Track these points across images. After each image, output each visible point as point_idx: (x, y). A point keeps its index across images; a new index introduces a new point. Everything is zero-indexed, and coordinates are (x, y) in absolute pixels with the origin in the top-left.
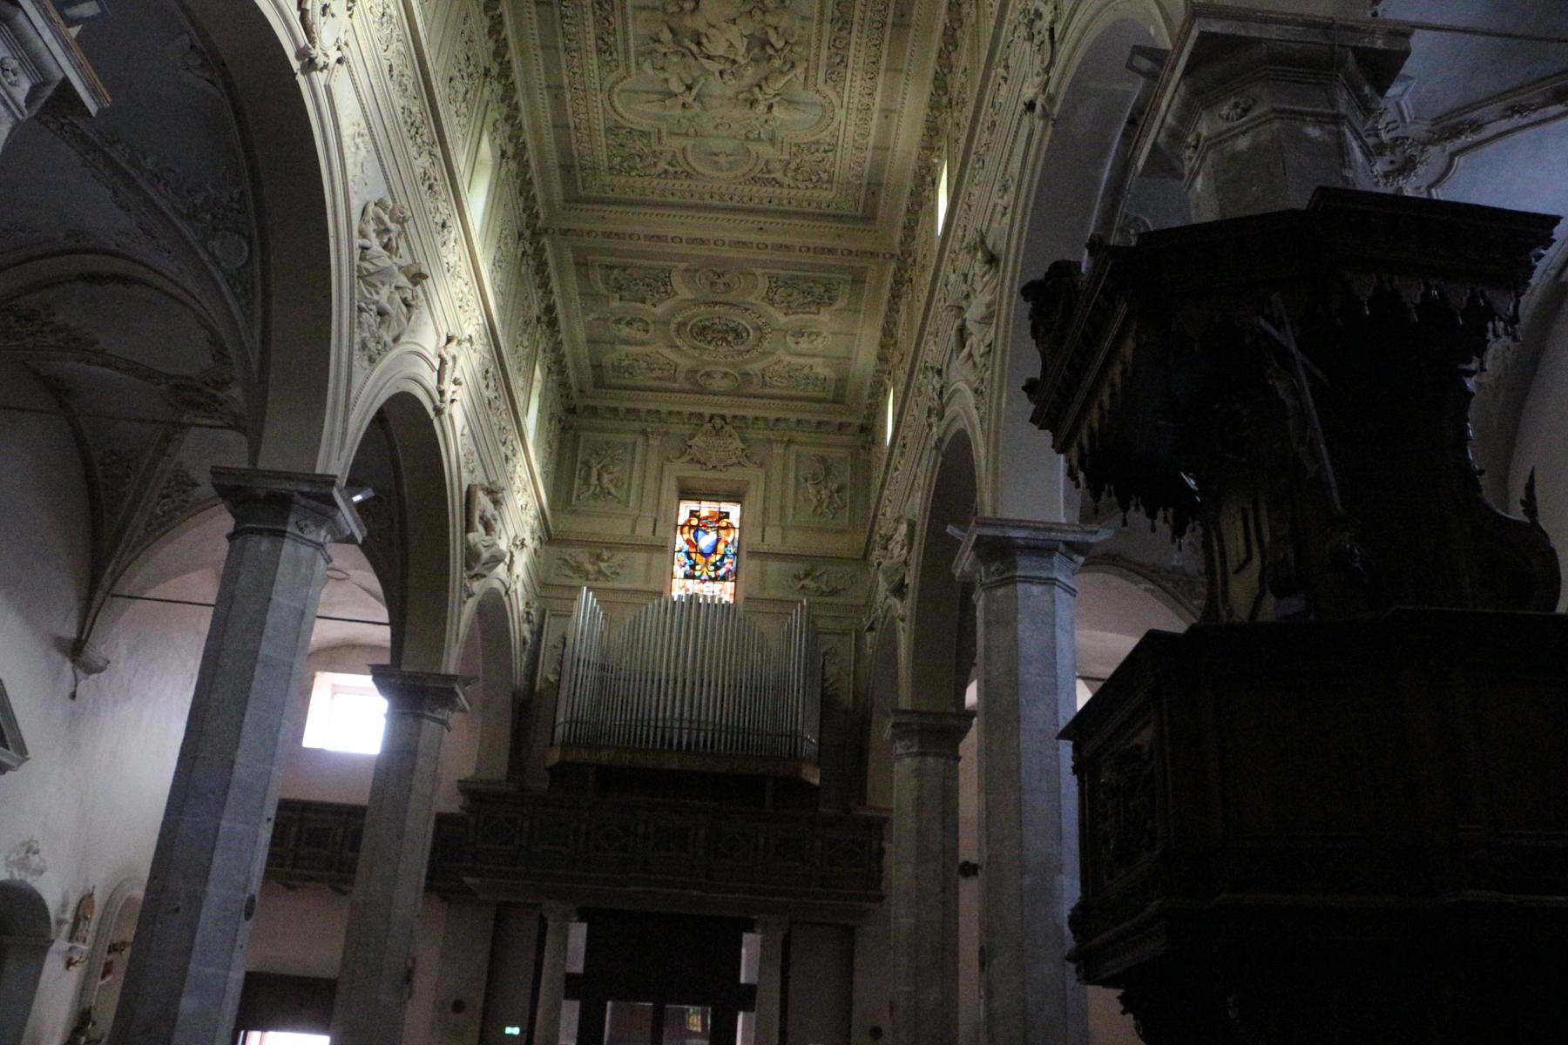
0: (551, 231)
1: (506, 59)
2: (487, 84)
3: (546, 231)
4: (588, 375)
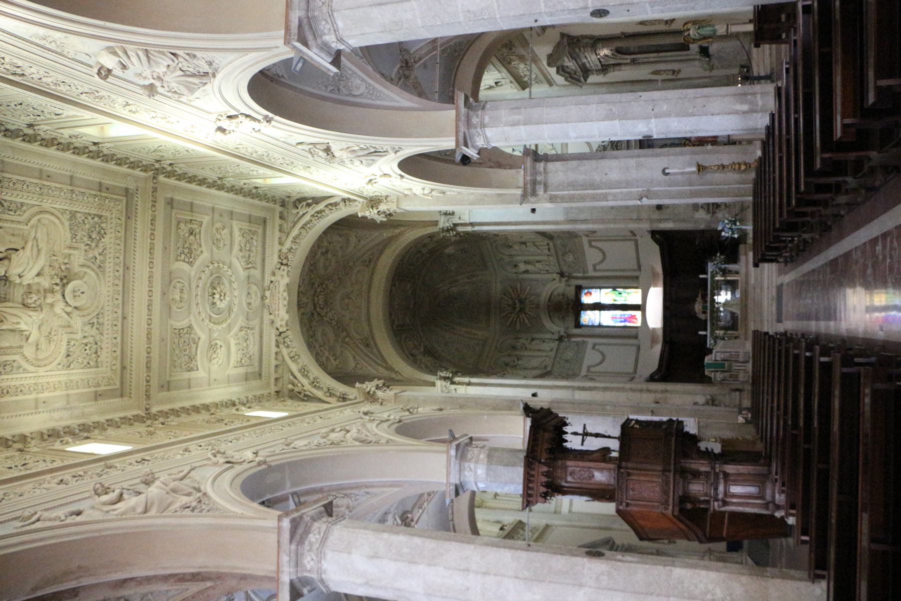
0: (147, 406)
1: (10, 438)
2: (28, 450)
3: (147, 409)
4: (255, 383)
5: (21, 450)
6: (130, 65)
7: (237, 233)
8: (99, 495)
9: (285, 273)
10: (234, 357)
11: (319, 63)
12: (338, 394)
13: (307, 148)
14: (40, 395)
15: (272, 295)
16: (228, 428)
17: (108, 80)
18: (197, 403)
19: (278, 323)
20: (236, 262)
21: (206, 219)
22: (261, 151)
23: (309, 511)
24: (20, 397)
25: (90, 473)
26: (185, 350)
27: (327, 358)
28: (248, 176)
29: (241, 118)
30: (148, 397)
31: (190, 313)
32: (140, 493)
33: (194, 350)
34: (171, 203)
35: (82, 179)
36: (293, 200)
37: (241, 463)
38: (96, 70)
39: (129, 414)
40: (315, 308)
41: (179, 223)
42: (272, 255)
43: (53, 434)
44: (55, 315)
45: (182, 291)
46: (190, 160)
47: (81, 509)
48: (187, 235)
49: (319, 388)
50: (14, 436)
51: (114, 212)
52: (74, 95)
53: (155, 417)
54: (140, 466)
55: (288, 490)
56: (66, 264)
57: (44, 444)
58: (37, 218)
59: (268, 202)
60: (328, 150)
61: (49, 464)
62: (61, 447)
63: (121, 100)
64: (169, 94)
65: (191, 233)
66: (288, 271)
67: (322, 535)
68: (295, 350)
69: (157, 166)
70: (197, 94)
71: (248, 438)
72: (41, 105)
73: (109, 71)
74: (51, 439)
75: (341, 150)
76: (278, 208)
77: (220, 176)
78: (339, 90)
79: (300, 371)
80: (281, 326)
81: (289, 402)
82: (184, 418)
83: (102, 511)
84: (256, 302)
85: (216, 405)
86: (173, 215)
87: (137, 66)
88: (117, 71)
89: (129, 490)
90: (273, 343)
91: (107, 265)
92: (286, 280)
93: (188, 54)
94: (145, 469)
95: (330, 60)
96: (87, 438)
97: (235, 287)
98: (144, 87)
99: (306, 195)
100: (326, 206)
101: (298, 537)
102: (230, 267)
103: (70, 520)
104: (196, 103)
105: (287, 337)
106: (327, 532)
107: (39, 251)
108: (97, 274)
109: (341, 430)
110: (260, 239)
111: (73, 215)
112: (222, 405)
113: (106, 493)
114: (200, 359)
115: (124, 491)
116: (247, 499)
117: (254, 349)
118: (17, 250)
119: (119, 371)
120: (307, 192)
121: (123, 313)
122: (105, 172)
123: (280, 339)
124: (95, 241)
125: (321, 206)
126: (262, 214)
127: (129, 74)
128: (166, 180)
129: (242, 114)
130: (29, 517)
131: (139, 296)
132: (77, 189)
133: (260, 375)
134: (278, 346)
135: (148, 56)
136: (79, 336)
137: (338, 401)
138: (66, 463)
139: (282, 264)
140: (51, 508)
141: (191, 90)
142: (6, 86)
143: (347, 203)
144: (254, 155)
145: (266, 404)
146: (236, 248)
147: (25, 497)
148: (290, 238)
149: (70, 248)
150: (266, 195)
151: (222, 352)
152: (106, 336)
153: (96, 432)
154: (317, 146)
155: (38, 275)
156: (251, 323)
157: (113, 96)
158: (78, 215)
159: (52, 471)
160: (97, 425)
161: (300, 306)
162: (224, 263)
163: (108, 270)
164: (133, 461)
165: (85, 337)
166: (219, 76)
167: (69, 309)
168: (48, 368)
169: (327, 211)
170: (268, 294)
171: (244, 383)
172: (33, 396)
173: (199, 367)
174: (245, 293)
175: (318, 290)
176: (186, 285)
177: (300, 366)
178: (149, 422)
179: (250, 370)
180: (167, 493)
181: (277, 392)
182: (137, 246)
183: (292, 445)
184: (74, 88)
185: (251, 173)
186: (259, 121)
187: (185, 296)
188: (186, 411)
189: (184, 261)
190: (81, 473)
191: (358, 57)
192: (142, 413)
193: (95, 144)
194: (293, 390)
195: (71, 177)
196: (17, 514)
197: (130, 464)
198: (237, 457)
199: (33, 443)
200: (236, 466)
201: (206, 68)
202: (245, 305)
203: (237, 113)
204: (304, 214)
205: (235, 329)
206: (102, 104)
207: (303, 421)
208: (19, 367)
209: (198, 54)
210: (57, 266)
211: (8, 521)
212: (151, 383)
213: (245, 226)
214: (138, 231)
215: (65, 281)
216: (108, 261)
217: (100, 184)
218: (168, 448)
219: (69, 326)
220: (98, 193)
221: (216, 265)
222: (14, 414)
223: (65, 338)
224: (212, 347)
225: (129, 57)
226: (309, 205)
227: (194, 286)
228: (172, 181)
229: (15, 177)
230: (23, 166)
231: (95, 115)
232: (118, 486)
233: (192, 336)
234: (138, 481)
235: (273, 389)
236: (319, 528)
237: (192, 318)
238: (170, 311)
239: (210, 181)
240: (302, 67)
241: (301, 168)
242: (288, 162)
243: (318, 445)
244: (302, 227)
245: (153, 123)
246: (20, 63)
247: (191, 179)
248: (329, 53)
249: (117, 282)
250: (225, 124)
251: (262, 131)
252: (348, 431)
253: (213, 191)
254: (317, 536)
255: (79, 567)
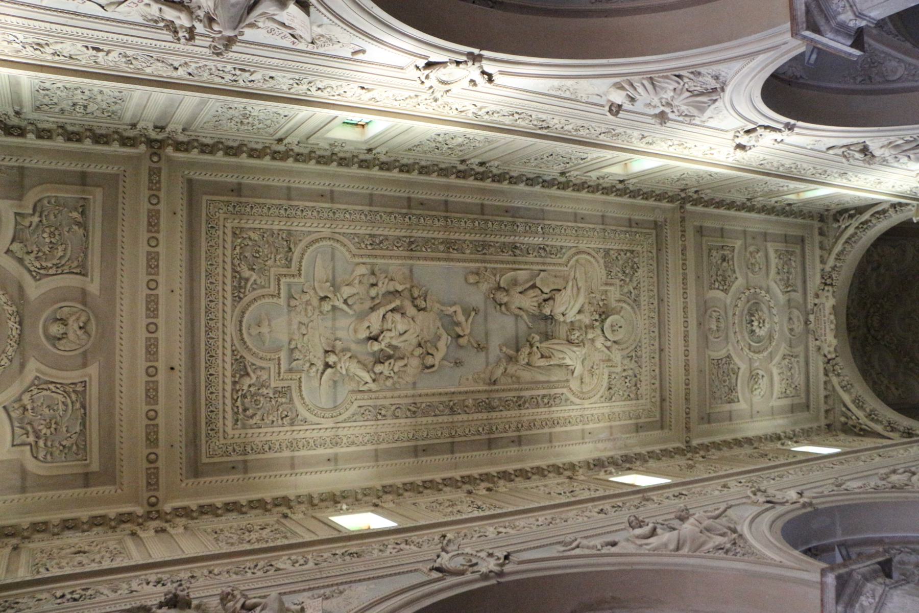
5: (570, 478)
6: (638, 97)
7: (772, 255)
8: (633, 528)
9: (830, 294)
10: (777, 388)
11: (836, 49)
12: (902, 429)
13: (840, 151)
14: (587, 427)
15: (817, 319)
16: (772, 464)
17: (620, 115)
18: (739, 436)
19: (826, 350)
20: (773, 285)
21: (738, 244)
22: (788, 163)
23: (860, 568)
24: (568, 428)
25: (628, 504)
26: (725, 381)
27: (887, 387)
28: (779, 193)
29: (760, 131)
30: (688, 429)
31: (728, 343)
32: (674, 529)
33: (734, 381)
34: (700, 231)
35: (612, 218)
36: (832, 213)
37: (782, 504)
38: (607, 108)
39: (670, 446)
40: (869, 330)
41: (710, 250)
42: (814, 274)
43: (598, 464)
44: (596, 349)
45: (718, 320)
46: (716, 185)
47: (616, 540)
48: (719, 262)
49: (877, 421)
50: (532, 468)
51: (645, 246)
52: (594, 137)
53: (695, 450)
54: (677, 501)
55: (840, 538)
56: (603, 300)
57: (590, 473)
58: (574, 259)
59: (804, 218)
60: (865, 150)
61: (592, 493)
62: (605, 477)
63: (636, 134)
64: (681, 119)
65: (724, 259)
66: (834, 292)
67: (877, 599)
68: (847, 378)
69: (683, 195)
70: (708, 113)
71: (793, 476)
72: (568, 153)
73: (620, 106)
74: (597, 468)
75: (882, 147)
76: (817, 224)
77: (749, 197)
78: (870, 78)
79: (854, 402)
80: (829, 352)
81: (842, 436)
82: (726, 452)
83: (636, 544)
84: (799, 327)
85: (760, 439)
86: (704, 242)
87: (644, 96)
88: (627, 105)
89: (663, 524)
90: (822, 371)
91: (642, 299)
92: (831, 302)
93: (692, 73)
94: (680, 504)
95: (850, 43)
96: (630, 469)
97: (775, 312)
98: (655, 116)
99: (847, 206)
100: (872, 215)
101: (845, 598)
102: (768, 292)
103: (605, 550)
104: (711, 123)
105: (836, 364)
106: (883, 596)
107: (578, 289)
108: (633, 308)
109: (905, 472)
110: (799, 259)
111: (607, 252)
112: (766, 439)
113: (641, 527)
114: (741, 390)
115: (659, 526)
116: (788, 545)
117: (799, 379)
118: (560, 290)
119: (658, 403)
120: (848, 203)
121: (660, 345)
122: (633, 207)
123: (829, 367)
124: (629, 276)
125: (866, 216)
126: (798, 232)
127: (639, 106)
128: (693, 208)
129: (760, 126)
130: (571, 543)
131: (675, 328)
132: (608, 228)
133: (808, 407)
134: (826, 375)
135: (653, 84)
136: (619, 369)
137: (902, 437)
138: (607, 493)
139: (826, 284)
140: (590, 537)
141: (702, 109)
142: (538, 140)
143: (898, 208)
144: (781, 169)
145: (816, 438)
146: (773, 271)
147: (569, 522)
148: (833, 256)
149: (606, 284)
150: (801, 211)
151: (764, 383)
152: (644, 369)
153: (638, 463)
154: (852, 148)
155: (579, 312)
156: (794, 350)
157: (629, 132)
158: (612, 252)
159: (593, 500)
160: (639, 457)
161: (850, 328)
162: (761, 288)
163: (643, 303)
164: (671, 495)
165: (624, 370)
166: (728, 89)
167: (609, 344)
168: (592, 400)
169: (874, 221)
170: (812, 318)
171: (790, 415)
172: (580, 427)
173: (741, 399)
174: (786, 319)
175: (872, 310)
176: (723, 313)
177: (854, 395)
178: (689, 455)
179: (796, 401)
180: (701, 532)
181: (829, 426)
182: (670, 277)
183: (844, 487)
184: (592, 131)
185: (781, 189)
186: (780, 130)
187: (722, 325)
188: (727, 444)
189: (718, 289)
190: (620, 504)
191: (890, 37)
192: (682, 446)
193: (621, 182)
194: (846, 423)
195: (603, 216)
196: (561, 539)
197: (668, 498)
198: (779, 496)
199: (581, 471)
200: (778, 507)
201: (713, 84)
202: (786, 330)
203: (754, 126)
204: (847, 227)
205: (778, 358)
206: (620, 141)
207: (858, 459)
208: (567, 400)
209: (702, 70)
210: (596, 303)
211: (553, 544)
212: (691, 415)
213: (781, 246)
214: (669, 262)
215: (603, 317)
216: (642, 294)
217: (630, 220)
218: (706, 483)
219: (609, 360)
220: (629, 229)
221: (752, 291)
222: (564, 443)
223: (606, 371)
224: (753, 377)
225: (635, 89)
226: (851, 216)
227: (730, 314)
228: (700, 209)
229: (554, 223)
230: (561, 212)
231: (616, 153)
232: (653, 520)
233: (732, 366)
234: (672, 516)
235: (823, 422)
236: (873, 591)
237: (730, 347)
238: (707, 342)
239: (738, 203)
240: (817, 59)
241: (836, 175)
242: (820, 171)
243: (876, 489)
244: (846, 242)
245: (671, 151)
246: (544, 117)
247: (719, 204)
248: (848, 35)
249: (652, 314)
250: (744, 140)
251: (785, 141)
252: (914, 474)
253: (743, 214)
254: (871, 600)
255: (613, 598)
